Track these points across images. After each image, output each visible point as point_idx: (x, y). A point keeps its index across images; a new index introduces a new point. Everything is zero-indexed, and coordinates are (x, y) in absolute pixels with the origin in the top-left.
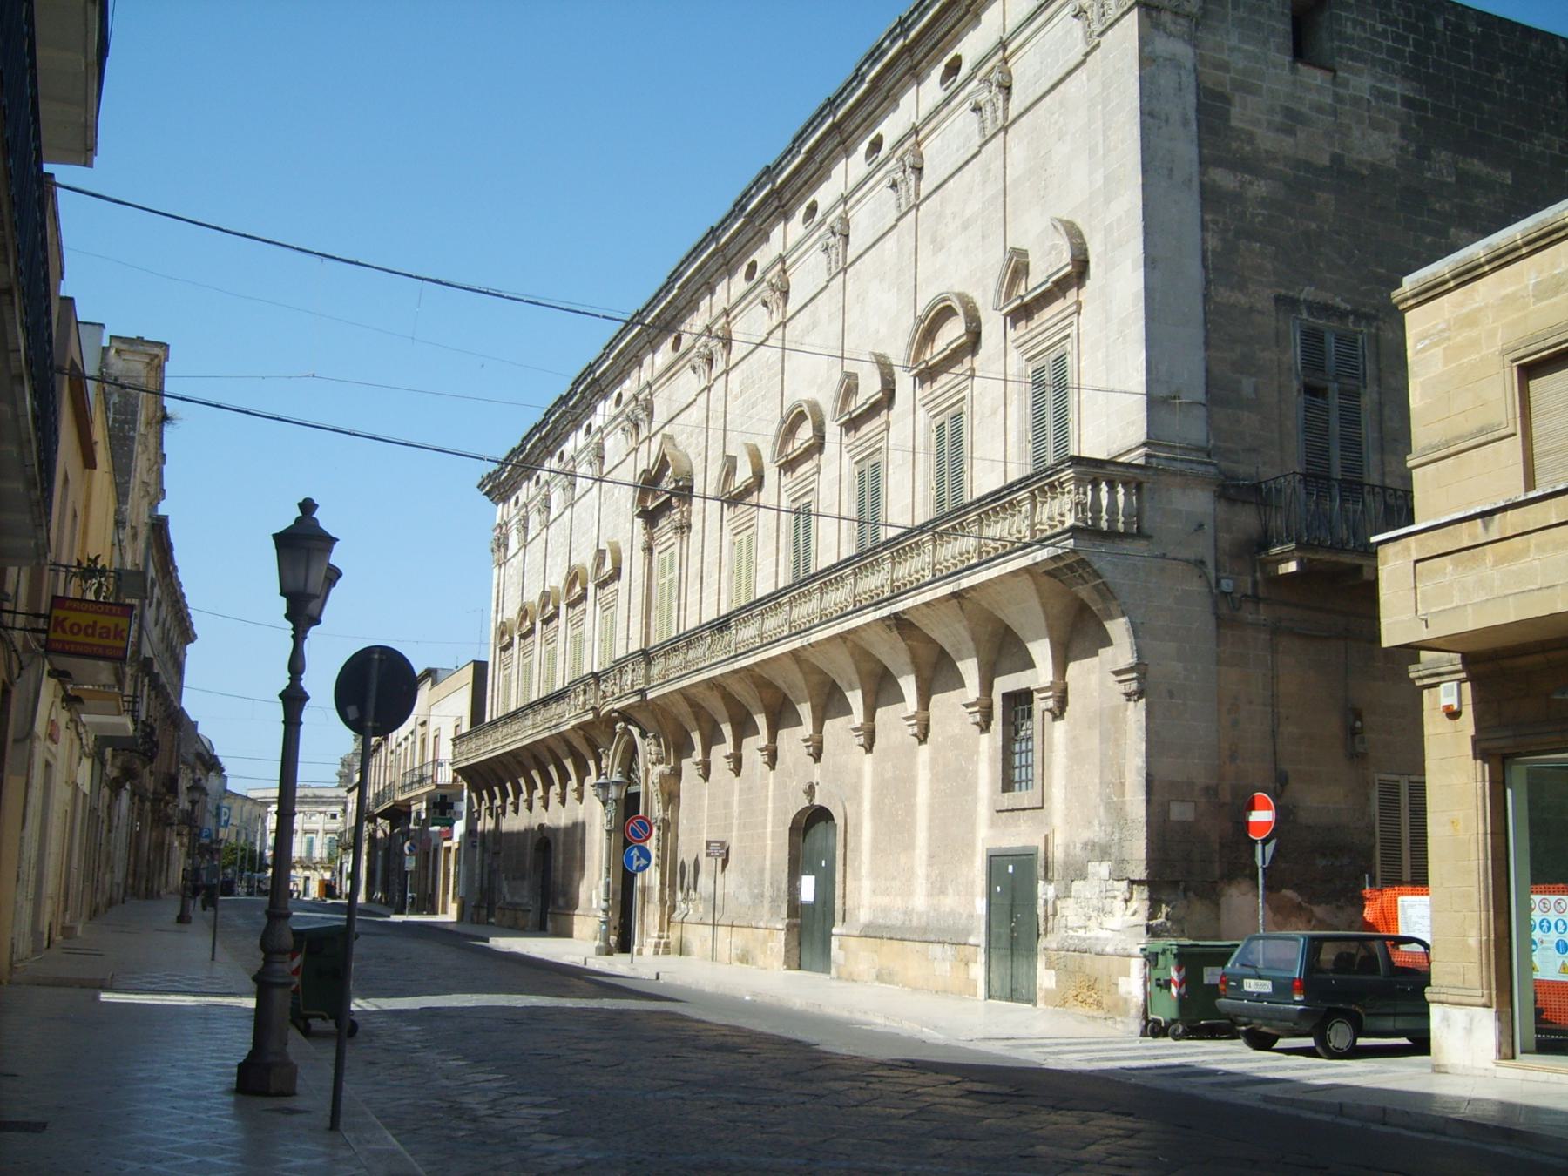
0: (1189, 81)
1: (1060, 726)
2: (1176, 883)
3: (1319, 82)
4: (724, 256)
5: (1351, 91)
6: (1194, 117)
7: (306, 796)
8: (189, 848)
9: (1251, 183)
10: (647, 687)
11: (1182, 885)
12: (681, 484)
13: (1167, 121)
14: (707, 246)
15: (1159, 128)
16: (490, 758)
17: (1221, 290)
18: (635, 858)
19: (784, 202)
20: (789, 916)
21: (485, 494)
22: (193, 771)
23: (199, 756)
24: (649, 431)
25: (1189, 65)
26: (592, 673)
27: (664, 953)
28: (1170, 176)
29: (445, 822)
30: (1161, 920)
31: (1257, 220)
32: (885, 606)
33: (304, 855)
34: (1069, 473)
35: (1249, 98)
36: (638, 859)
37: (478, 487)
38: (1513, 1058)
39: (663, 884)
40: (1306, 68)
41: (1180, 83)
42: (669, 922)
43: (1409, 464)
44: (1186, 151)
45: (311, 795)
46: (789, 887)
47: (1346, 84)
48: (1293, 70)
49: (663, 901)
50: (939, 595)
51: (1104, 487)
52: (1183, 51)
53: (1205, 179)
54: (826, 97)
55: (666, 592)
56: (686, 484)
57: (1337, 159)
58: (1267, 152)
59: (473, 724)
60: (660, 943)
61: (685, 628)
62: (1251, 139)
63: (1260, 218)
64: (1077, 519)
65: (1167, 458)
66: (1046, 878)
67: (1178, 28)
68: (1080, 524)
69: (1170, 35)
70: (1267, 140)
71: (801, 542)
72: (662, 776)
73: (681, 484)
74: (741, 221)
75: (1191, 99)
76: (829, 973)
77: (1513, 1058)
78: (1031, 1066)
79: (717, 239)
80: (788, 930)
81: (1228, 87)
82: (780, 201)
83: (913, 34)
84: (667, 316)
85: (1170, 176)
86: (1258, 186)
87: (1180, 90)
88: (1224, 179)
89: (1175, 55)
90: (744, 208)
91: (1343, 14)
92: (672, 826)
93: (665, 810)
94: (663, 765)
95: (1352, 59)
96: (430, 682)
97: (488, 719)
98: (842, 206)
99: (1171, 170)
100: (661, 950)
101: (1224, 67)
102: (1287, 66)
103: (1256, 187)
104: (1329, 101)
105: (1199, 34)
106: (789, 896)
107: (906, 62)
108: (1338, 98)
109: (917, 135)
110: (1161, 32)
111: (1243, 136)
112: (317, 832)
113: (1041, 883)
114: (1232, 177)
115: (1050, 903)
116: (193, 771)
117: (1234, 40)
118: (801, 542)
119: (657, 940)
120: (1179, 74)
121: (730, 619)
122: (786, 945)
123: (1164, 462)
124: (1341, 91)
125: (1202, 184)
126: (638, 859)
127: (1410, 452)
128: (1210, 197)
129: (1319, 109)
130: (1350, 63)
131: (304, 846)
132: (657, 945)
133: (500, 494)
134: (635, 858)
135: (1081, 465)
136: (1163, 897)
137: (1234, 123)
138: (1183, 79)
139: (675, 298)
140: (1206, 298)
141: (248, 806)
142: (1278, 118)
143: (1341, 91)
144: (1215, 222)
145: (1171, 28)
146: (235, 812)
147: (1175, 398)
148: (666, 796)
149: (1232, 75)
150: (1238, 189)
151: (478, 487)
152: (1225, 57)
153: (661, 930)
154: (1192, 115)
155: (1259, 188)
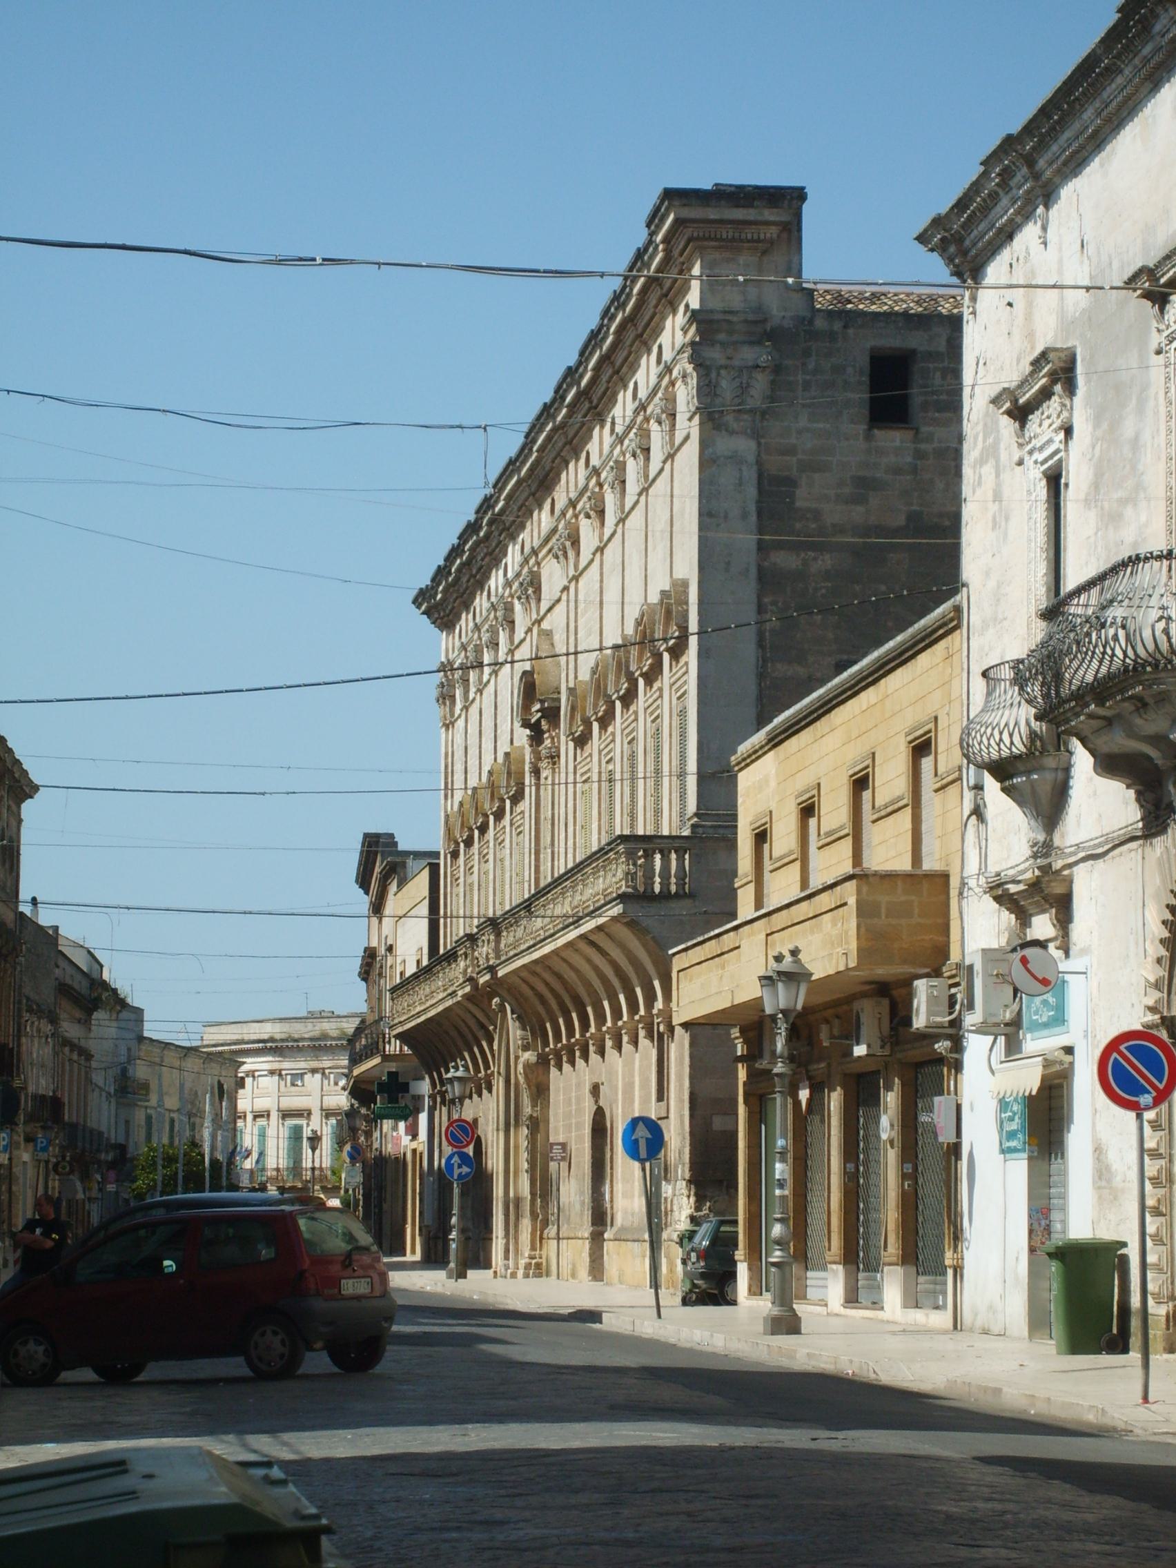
0: (750, 474)
1: (637, 1055)
2: (721, 1182)
3: (898, 443)
4: (565, 434)
5: (935, 445)
6: (754, 509)
7: (324, 1036)
8: (235, 1115)
9: (815, 559)
10: (498, 962)
11: (725, 1184)
12: (546, 705)
13: (726, 517)
14: (544, 425)
15: (718, 525)
16: (418, 1024)
17: (779, 666)
18: (456, 1166)
19: (595, 402)
20: (593, 1224)
21: (423, 613)
22: (54, 1020)
23: (64, 990)
24: (538, 613)
25: (751, 458)
26: (466, 935)
27: (535, 1276)
28: (727, 570)
29: (398, 1112)
30: (705, 1211)
31: (819, 594)
32: (587, 922)
33: (283, 1164)
34: (621, 848)
35: (816, 476)
36: (460, 1166)
37: (414, 602)
38: (761, 1295)
39: (533, 1194)
40: (883, 432)
41: (741, 478)
42: (541, 1238)
43: (736, 885)
44: (746, 539)
45: (334, 1033)
46: (593, 1193)
47: (929, 438)
48: (868, 437)
49: (534, 1215)
50: (558, 945)
51: (673, 856)
52: (745, 446)
53: (766, 564)
54: (612, 291)
55: (75, 1084)
56: (553, 705)
57: (913, 517)
58: (834, 525)
59: (430, 957)
60: (530, 1264)
61: (511, 904)
62: (817, 515)
63: (824, 591)
64: (627, 886)
65: (712, 827)
66: (666, 1179)
67: (742, 424)
68: (630, 890)
69: (732, 433)
70: (834, 514)
71: (923, 644)
72: (527, 1066)
73: (546, 705)
74: (564, 411)
75: (752, 491)
76: (487, 1265)
77: (761, 1295)
78: (475, 1307)
79: (554, 417)
80: (592, 1239)
81: (795, 469)
82: (591, 402)
83: (628, 309)
84: (540, 472)
85: (727, 570)
86: (823, 560)
87: (740, 485)
88: (786, 560)
89: (736, 452)
90: (563, 398)
91: (931, 365)
92: (542, 1126)
93: (534, 1106)
94: (530, 1052)
95: (938, 412)
96: (396, 881)
97: (442, 951)
98: (619, 447)
99: (728, 563)
100: (531, 1272)
101: (791, 451)
102: (861, 437)
103: (820, 562)
104: (909, 459)
105: (765, 423)
106: (593, 1202)
107: (630, 334)
108: (919, 455)
109: (645, 411)
110: (724, 432)
111: (808, 516)
112: (310, 1113)
113: (664, 1183)
114: (794, 557)
115: (669, 1200)
116: (54, 1020)
117: (803, 422)
118: (923, 644)
119: (527, 1260)
120: (740, 469)
121: (531, 904)
122: (590, 1255)
123: (711, 831)
124: (923, 446)
125: (760, 569)
126: (460, 1166)
127: (736, 876)
128: (767, 580)
129: (897, 471)
130: (937, 415)
131: (284, 1144)
132: (528, 1267)
133: (442, 618)
134: (456, 1166)
135: (629, 841)
136: (709, 1194)
137: (798, 504)
138: (745, 473)
139: (537, 461)
140: (761, 676)
141: (192, 1064)
142: (847, 490)
143: (923, 446)
144: (774, 603)
145: (735, 426)
146: (170, 1077)
147: (723, 772)
148: (534, 1088)
149: (800, 456)
150: (800, 567)
151: (414, 602)
152: (793, 441)
153: (533, 1248)
154: (752, 508)
155: (826, 562)
